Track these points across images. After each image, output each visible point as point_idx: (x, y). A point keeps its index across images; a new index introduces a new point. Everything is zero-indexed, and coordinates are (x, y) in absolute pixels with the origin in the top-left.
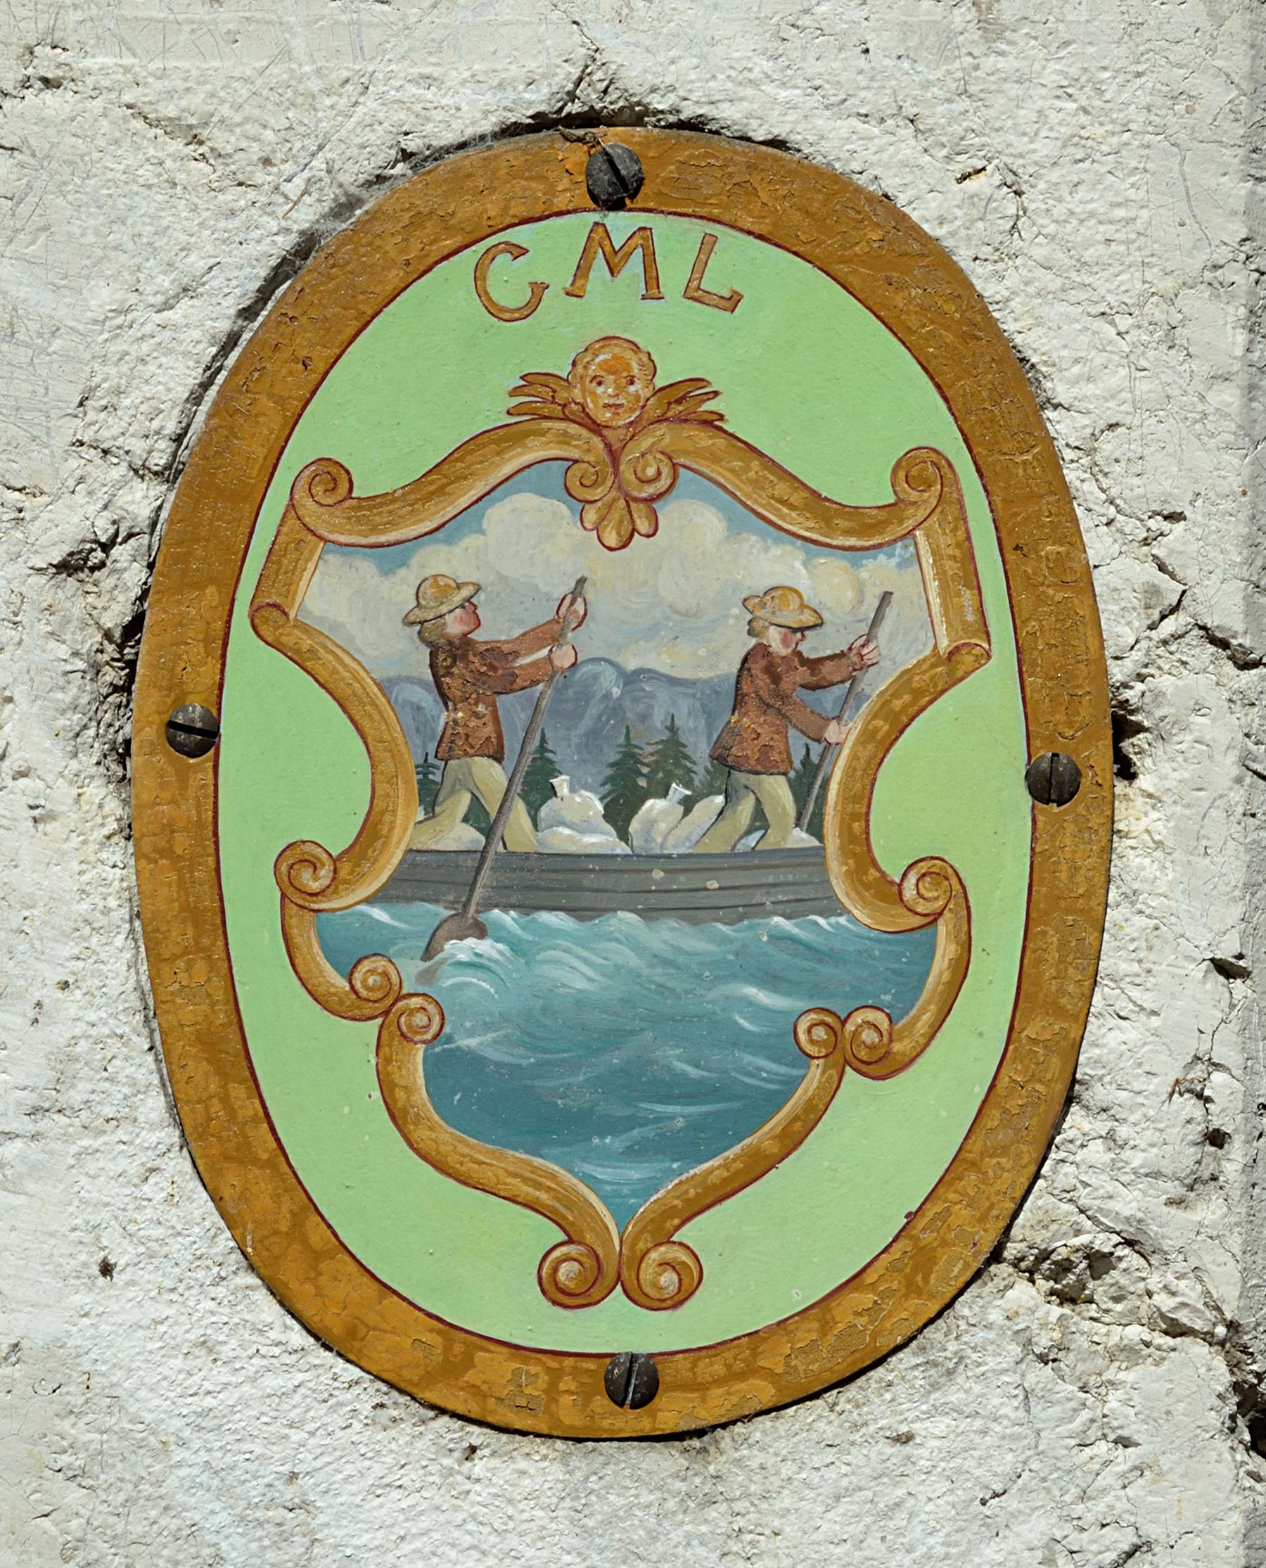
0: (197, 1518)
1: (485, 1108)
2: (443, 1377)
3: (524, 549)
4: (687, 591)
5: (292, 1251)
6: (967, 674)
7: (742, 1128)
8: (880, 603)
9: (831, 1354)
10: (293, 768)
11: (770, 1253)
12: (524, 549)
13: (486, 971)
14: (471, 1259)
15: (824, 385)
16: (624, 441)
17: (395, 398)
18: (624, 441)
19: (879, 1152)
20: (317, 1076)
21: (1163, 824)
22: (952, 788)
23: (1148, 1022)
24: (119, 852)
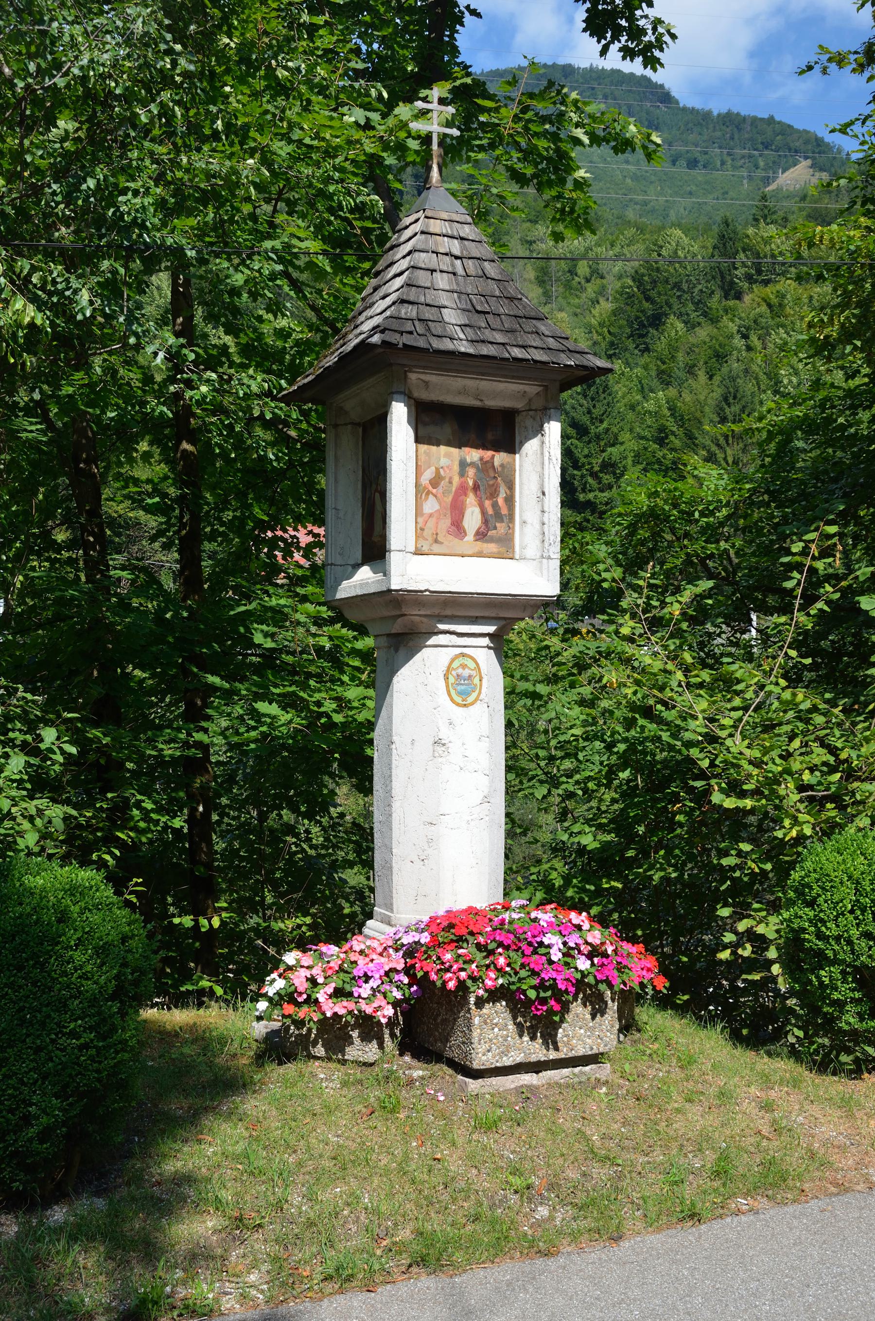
0: (675, 307)
1: (460, 694)
2: (458, 705)
3: (460, 671)
4: (466, 673)
5: (452, 700)
6: (372, 828)
7: (469, 694)
8: (474, 673)
9: (472, 704)
10: (452, 680)
11: (470, 699)
12: (460, 671)
13: (459, 688)
14: (459, 700)
15: (471, 664)
16: (464, 666)
17: (456, 664)
18: (464, 666)
19: (474, 695)
20: (453, 692)
21: (484, 681)
22: (476, 681)
23: (484, 690)
24: (587, 65)
